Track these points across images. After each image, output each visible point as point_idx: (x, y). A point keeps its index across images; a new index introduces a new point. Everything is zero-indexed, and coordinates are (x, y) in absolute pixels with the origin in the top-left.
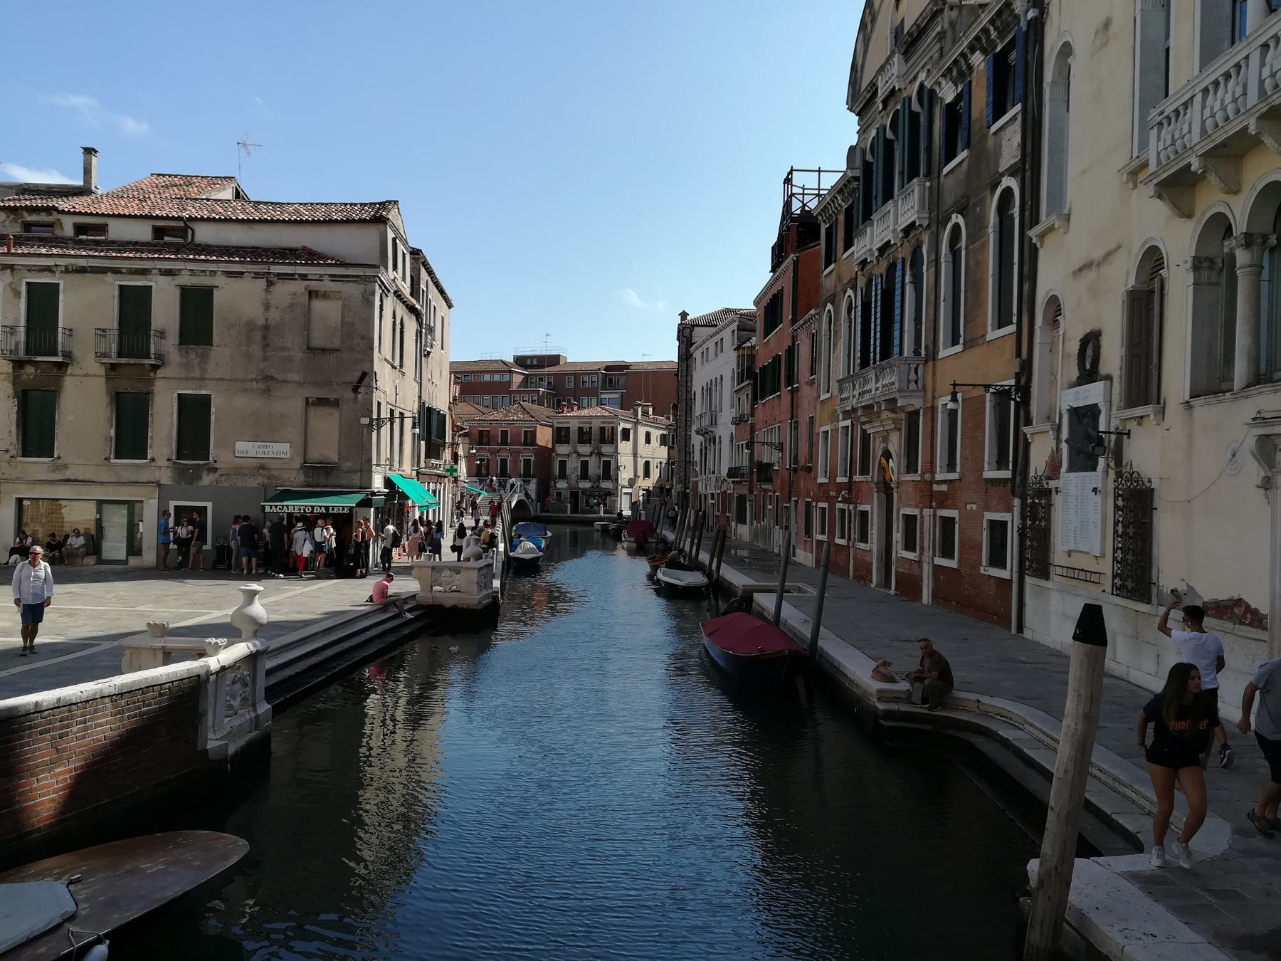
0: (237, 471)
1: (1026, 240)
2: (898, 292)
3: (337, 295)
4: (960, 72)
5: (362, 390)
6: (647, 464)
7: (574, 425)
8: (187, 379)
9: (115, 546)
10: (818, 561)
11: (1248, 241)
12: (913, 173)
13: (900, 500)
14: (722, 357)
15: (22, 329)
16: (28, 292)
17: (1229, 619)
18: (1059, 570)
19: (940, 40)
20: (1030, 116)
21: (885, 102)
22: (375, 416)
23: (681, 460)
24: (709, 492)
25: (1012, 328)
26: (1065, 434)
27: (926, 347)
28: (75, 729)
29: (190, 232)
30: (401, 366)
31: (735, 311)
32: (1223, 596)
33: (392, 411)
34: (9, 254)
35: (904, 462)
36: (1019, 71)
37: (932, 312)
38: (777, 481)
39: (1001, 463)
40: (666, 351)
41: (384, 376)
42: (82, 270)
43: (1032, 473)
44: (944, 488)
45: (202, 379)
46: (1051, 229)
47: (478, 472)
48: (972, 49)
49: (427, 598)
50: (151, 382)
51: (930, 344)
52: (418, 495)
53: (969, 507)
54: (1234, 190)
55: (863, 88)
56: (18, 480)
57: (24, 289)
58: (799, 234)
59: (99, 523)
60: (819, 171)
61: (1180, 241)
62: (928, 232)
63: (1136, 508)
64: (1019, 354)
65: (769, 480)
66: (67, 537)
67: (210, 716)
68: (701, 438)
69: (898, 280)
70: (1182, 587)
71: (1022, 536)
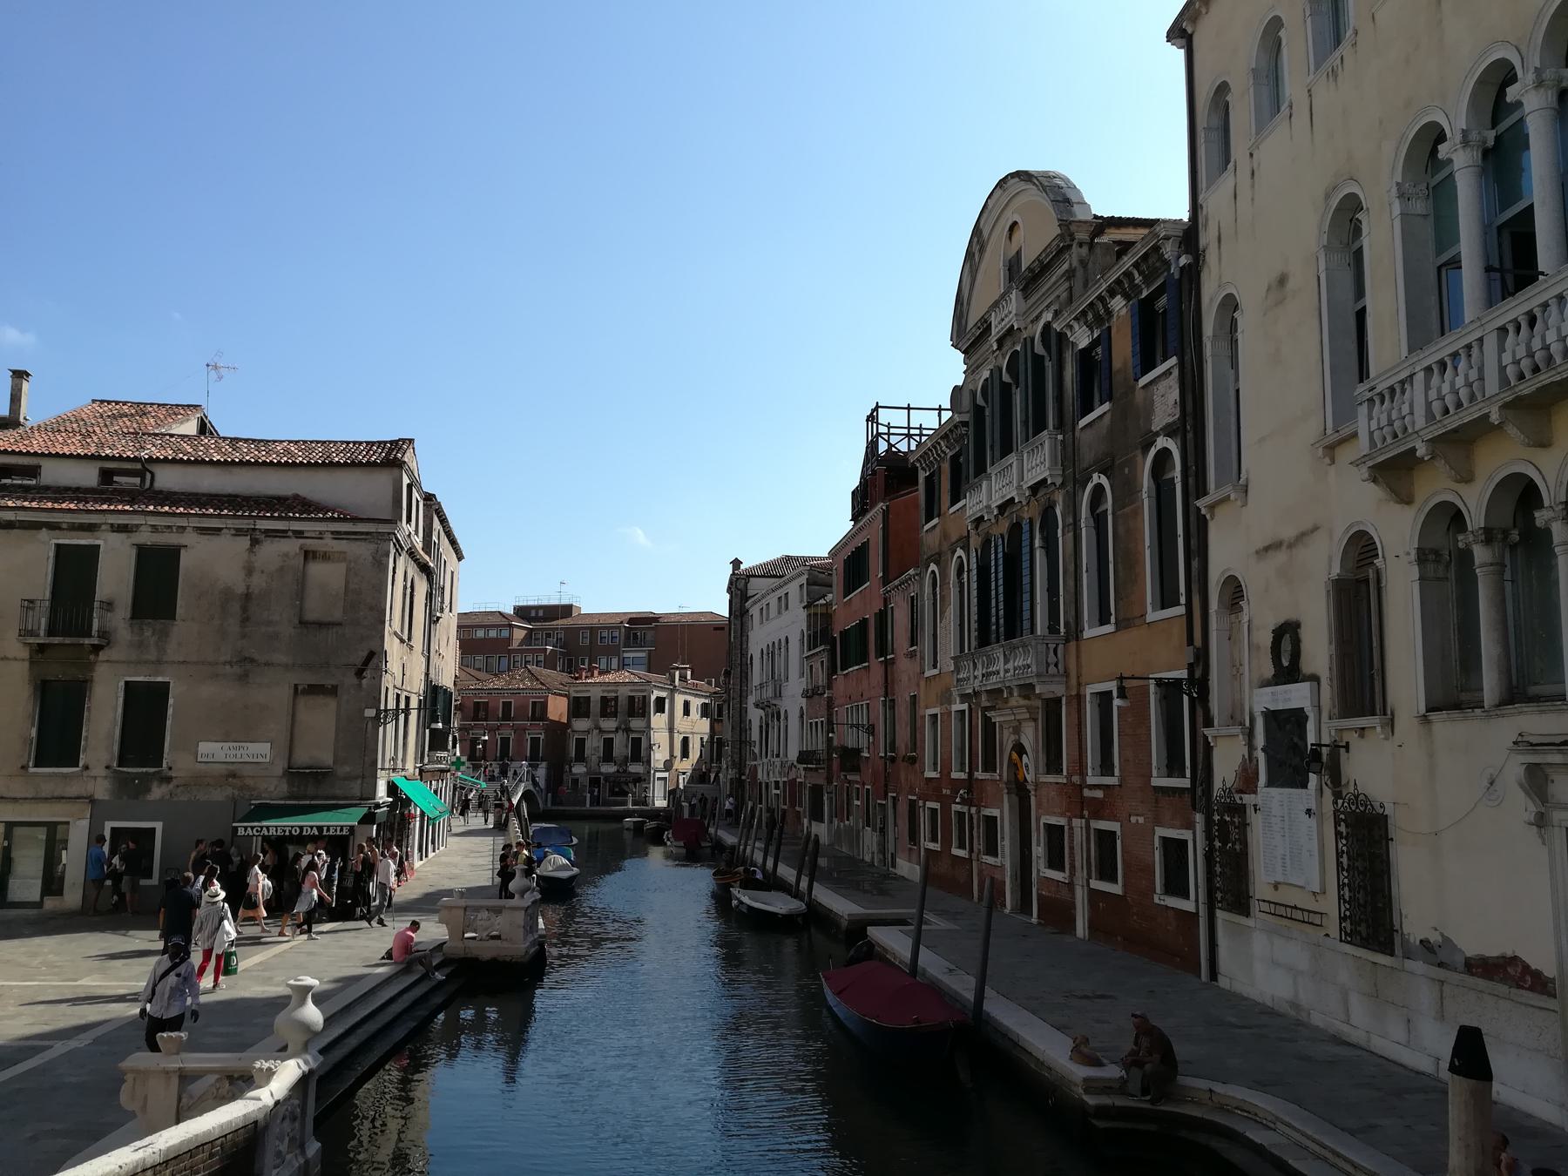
0: (199, 780)
1: (1192, 509)
2: (1026, 557)
3: (342, 557)
4: (1097, 316)
5: (368, 674)
6: (685, 741)
7: (595, 694)
8: (139, 662)
11: (1489, 536)
13: (1039, 805)
14: (786, 616)
17: (1504, 981)
18: (1265, 907)
21: (1000, 342)
24: (773, 779)
25: (1180, 610)
26: (1260, 740)
27: (1067, 624)
29: (148, 476)
31: (796, 559)
32: (1492, 952)
37: (1072, 583)
39: (1174, 767)
40: (721, 606)
41: (392, 646)
43: (1217, 784)
44: (1099, 794)
45: (159, 662)
48: (1112, 292)
49: (456, 949)
50: (91, 666)
51: (1072, 621)
52: (423, 797)
53: (1133, 819)
54: (1467, 478)
55: (970, 325)
60: (909, 408)
61: (1399, 534)
62: (1062, 492)
63: (1365, 839)
64: (1190, 641)
65: (856, 769)
69: (1025, 543)
70: (1434, 938)
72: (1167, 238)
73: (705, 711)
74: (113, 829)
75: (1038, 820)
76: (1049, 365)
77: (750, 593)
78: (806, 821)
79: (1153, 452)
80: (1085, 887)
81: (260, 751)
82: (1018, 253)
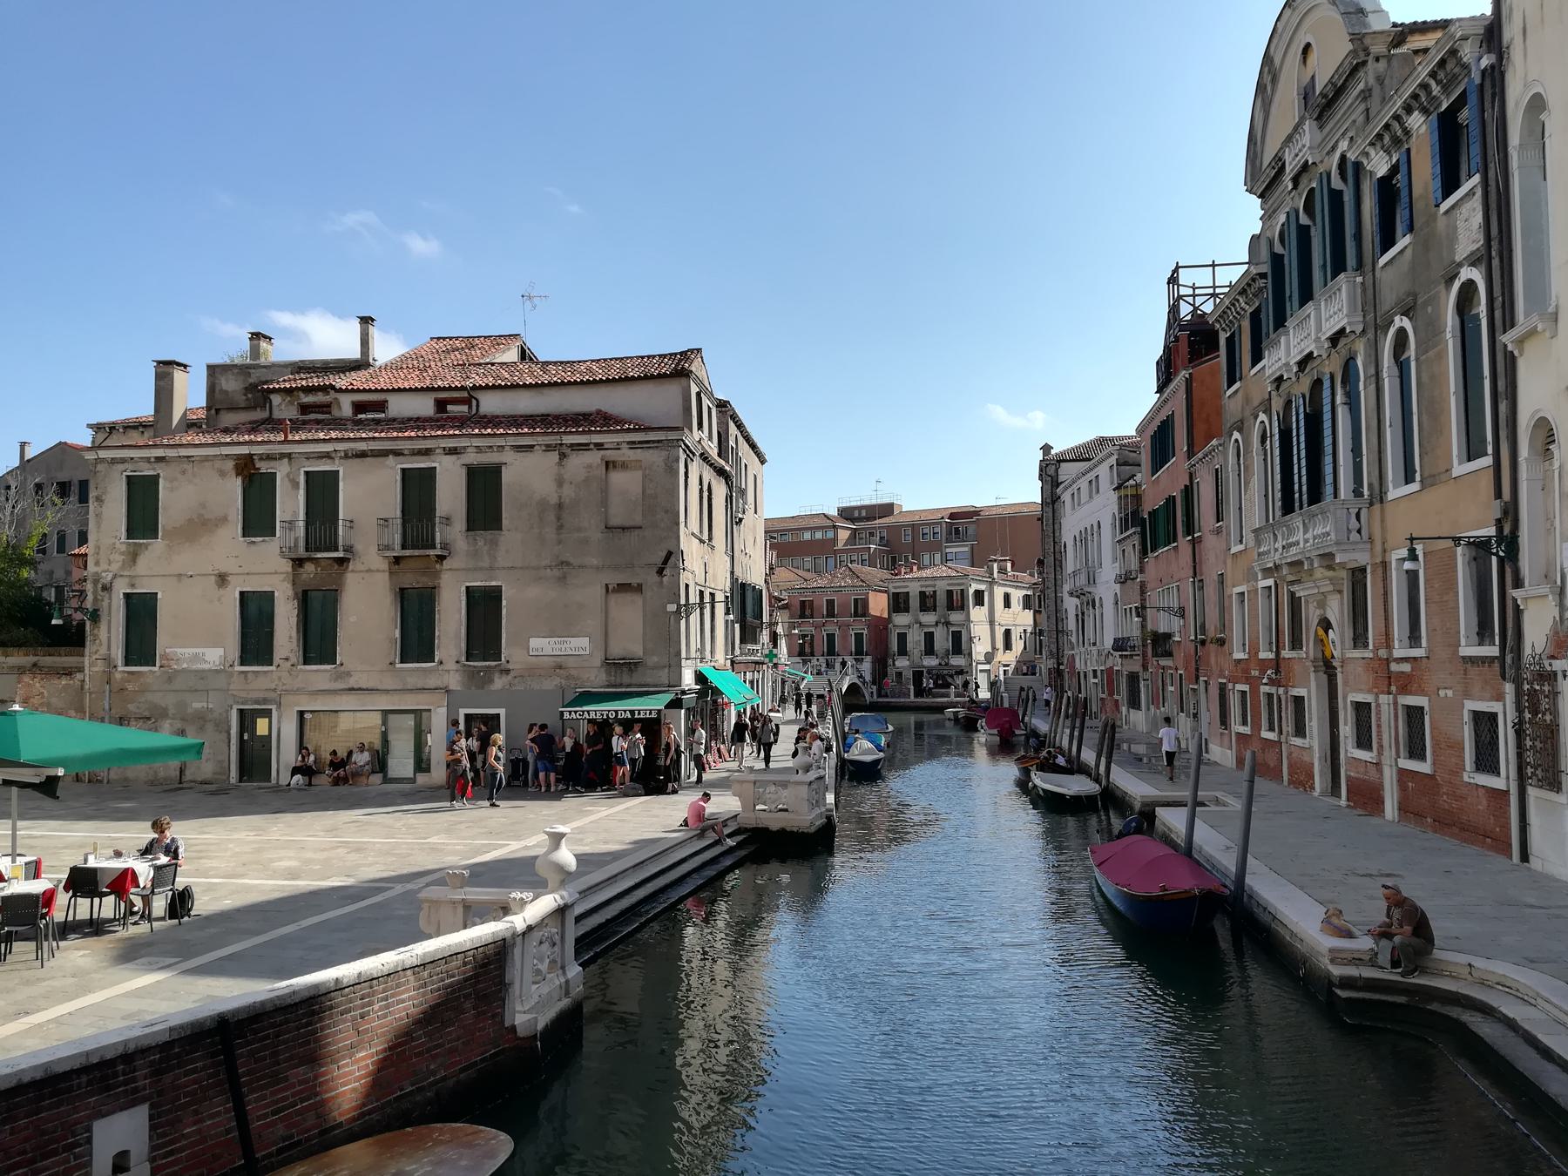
0: (532, 672)
1: (1499, 348)
3: (638, 465)
4: (1394, 137)
6: (1007, 633)
7: (914, 589)
9: (401, 763)
10: (1240, 762)
12: (1338, 266)
13: (1346, 683)
14: (1098, 499)
15: (301, 524)
16: (307, 482)
19: (1365, 99)
20: (1492, 189)
21: (1296, 181)
22: (683, 602)
23: (1050, 634)
24: (1090, 669)
25: (1487, 461)
27: (1370, 485)
28: (376, 1007)
30: (710, 539)
31: (1111, 439)
33: (701, 593)
34: (286, 441)
35: (1349, 634)
36: (1474, 131)
37: (1375, 440)
38: (1179, 655)
40: (1027, 491)
41: (690, 548)
42: (362, 455)
43: (1527, 651)
44: (1406, 667)
45: (491, 568)
46: (1533, 332)
47: (803, 652)
48: (1409, 109)
49: (750, 821)
50: (437, 574)
52: (736, 692)
53: (1442, 693)
55: (1265, 164)
56: (298, 691)
57: (302, 479)
58: (1191, 344)
59: (385, 735)
60: (1213, 265)
62: (1364, 340)
64: (1498, 495)
65: (1169, 654)
66: (350, 753)
67: (517, 985)
68: (1076, 601)
69: (1327, 400)
71: (1519, 733)
72: (1464, 38)
73: (1027, 603)
74: (467, 716)
75: (1345, 698)
76: (1348, 198)
77: (1061, 479)
78: (1124, 709)
79: (1457, 285)
80: (1389, 763)
81: (579, 645)
82: (1313, 77)
